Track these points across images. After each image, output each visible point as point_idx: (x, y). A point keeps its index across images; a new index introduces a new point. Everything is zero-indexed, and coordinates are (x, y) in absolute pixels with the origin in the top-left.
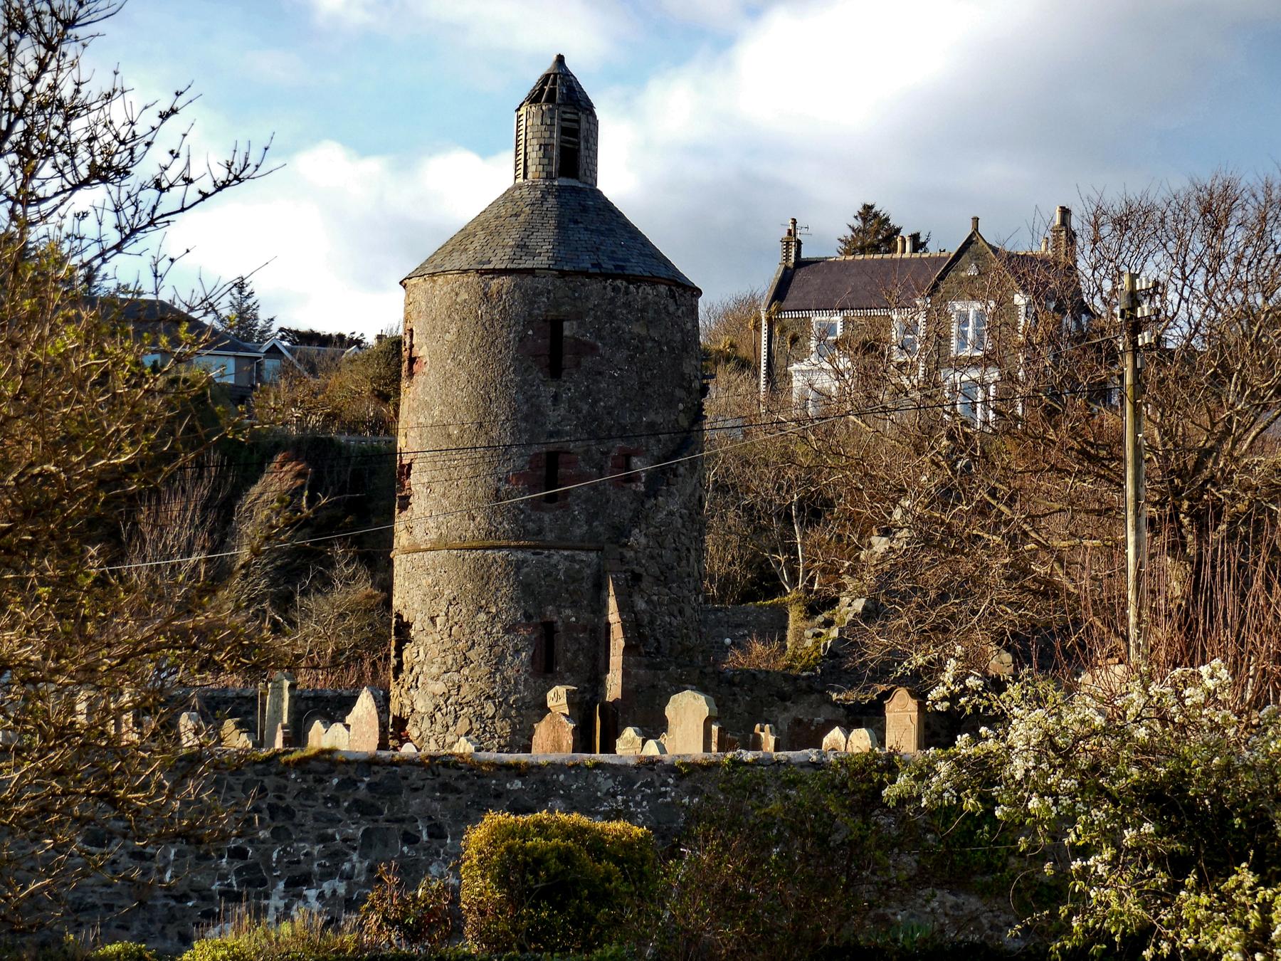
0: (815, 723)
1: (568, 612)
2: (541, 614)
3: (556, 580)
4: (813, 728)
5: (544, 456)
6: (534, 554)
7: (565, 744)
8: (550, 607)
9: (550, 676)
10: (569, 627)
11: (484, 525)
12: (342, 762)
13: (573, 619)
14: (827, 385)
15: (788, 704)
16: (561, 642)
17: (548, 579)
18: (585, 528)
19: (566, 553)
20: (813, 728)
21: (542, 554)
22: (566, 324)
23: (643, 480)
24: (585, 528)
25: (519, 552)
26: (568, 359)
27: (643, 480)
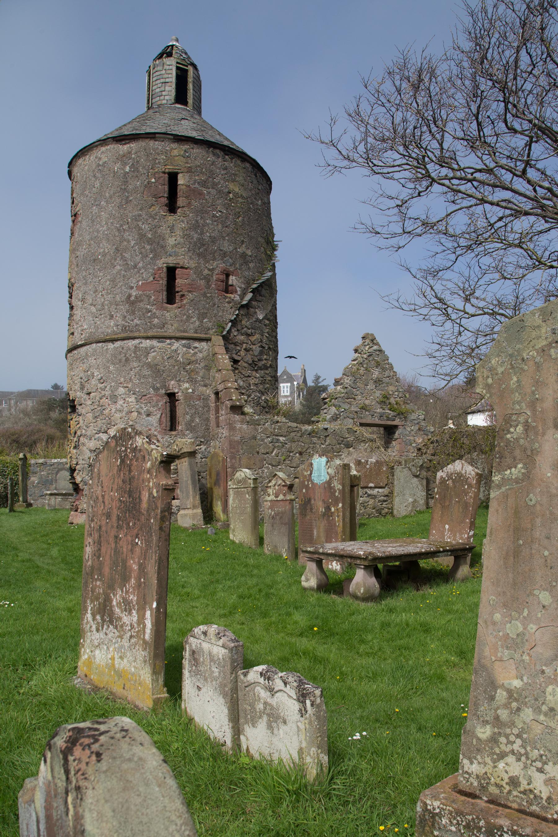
0: (369, 463)
1: (186, 385)
2: (164, 386)
3: (176, 361)
4: (368, 466)
5: (165, 270)
6: (158, 342)
7: (145, 496)
8: (173, 382)
9: (173, 433)
10: (188, 397)
11: (121, 322)
12: (486, 411)
13: (190, 391)
14: (61, 800)
15: (351, 449)
16: (180, 409)
17: (171, 361)
18: (197, 323)
19: (184, 342)
20: (368, 466)
21: (165, 342)
22: (180, 176)
23: (239, 293)
24: (197, 323)
25: (148, 341)
26: (181, 201)
27: (239, 293)
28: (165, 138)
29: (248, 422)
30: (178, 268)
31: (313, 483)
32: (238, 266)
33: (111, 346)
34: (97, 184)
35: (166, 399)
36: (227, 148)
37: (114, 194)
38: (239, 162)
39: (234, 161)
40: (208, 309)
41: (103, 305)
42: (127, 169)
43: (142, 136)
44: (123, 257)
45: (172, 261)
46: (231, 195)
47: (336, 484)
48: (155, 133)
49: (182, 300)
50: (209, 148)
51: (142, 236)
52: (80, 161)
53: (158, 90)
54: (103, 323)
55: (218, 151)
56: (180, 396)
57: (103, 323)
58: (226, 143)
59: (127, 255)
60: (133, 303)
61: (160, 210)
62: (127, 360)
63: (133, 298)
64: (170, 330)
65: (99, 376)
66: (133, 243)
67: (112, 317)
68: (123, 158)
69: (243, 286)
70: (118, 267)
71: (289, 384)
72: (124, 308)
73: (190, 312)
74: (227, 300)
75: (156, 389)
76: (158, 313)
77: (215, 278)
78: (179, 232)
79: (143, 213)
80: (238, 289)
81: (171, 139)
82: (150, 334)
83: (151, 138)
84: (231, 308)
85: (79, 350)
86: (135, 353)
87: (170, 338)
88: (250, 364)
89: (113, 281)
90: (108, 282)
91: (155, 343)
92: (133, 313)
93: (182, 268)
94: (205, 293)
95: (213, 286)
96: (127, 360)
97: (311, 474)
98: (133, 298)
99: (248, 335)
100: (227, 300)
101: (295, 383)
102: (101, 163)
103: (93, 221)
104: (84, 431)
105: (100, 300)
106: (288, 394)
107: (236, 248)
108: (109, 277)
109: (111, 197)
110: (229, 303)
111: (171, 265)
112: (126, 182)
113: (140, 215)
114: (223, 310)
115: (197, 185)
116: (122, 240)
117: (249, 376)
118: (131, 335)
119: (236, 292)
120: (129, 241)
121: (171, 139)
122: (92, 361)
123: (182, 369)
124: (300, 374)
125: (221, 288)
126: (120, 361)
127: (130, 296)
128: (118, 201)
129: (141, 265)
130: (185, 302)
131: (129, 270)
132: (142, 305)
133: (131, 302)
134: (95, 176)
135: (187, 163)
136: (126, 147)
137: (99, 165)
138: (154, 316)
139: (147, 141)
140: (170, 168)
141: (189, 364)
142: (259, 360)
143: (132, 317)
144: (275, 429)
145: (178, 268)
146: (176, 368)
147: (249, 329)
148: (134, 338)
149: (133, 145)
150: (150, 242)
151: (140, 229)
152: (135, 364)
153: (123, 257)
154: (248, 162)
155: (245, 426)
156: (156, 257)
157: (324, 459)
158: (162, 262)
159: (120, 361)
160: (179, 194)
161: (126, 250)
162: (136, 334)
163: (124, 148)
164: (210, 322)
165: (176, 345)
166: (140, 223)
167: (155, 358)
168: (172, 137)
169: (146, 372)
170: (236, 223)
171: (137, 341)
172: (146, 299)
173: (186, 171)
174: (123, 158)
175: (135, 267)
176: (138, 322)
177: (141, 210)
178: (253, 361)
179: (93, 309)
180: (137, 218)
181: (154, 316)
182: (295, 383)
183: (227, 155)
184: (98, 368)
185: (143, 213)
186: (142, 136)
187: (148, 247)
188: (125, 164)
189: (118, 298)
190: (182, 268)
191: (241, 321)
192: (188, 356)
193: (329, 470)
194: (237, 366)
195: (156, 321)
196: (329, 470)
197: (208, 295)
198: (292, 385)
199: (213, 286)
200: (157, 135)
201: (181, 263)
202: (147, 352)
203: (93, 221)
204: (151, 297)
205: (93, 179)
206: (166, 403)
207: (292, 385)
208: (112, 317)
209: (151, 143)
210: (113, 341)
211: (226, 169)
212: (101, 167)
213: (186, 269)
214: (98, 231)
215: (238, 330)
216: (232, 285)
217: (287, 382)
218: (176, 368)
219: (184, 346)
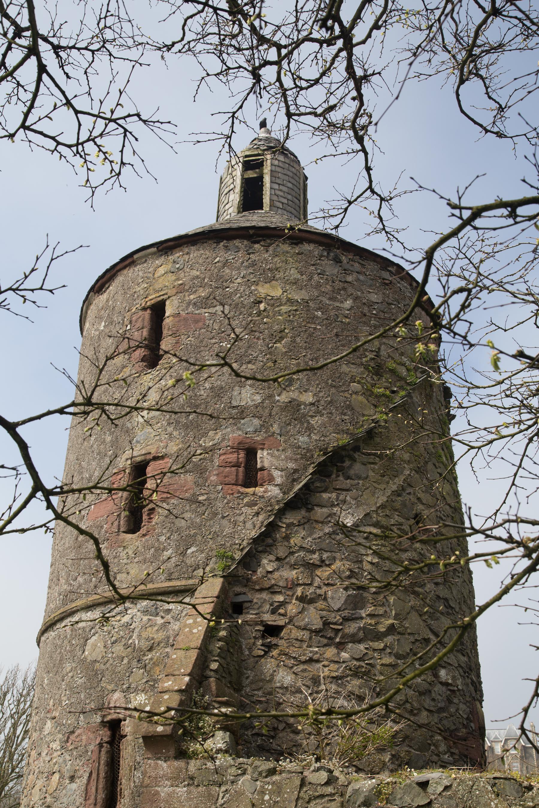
23: (279, 481)
28: (146, 256)
29: (192, 778)
30: (150, 460)
32: (275, 428)
35: (105, 734)
36: (251, 232)
38: (286, 247)
39: (271, 249)
40: (199, 527)
43: (118, 268)
46: (262, 306)
50: (218, 243)
55: (237, 242)
58: (312, 230)
69: (291, 465)
73: (162, 539)
74: (246, 500)
77: (217, 462)
80: (276, 474)
81: (153, 254)
83: (129, 265)
84: (257, 514)
88: (317, 632)
93: (156, 458)
94: (194, 494)
95: (213, 478)
99: (311, 567)
100: (246, 500)
107: (271, 396)
110: (251, 505)
111: (139, 459)
114: (235, 523)
115: (191, 309)
117: (311, 661)
119: (271, 479)
121: (153, 254)
123: (134, 663)
125: (232, 479)
135: (178, 279)
139: (125, 272)
140: (153, 298)
141: (151, 649)
142: (346, 619)
144: (263, 793)
145: (150, 460)
146: (125, 661)
147: (313, 552)
154: (310, 241)
155: (182, 790)
160: (165, 332)
164: (202, 552)
168: (154, 250)
170: (270, 351)
173: (174, 291)
178: (326, 624)
183: (258, 242)
186: (118, 268)
190: (156, 458)
191: (287, 538)
192: (151, 632)
194: (274, 641)
197: (201, 498)
199: (213, 478)
200: (135, 257)
201: (153, 451)
204: (102, 527)
206: (101, 745)
211: (253, 264)
213: (162, 458)
215: (278, 559)
216: (262, 469)
218: (125, 661)
219: (145, 612)
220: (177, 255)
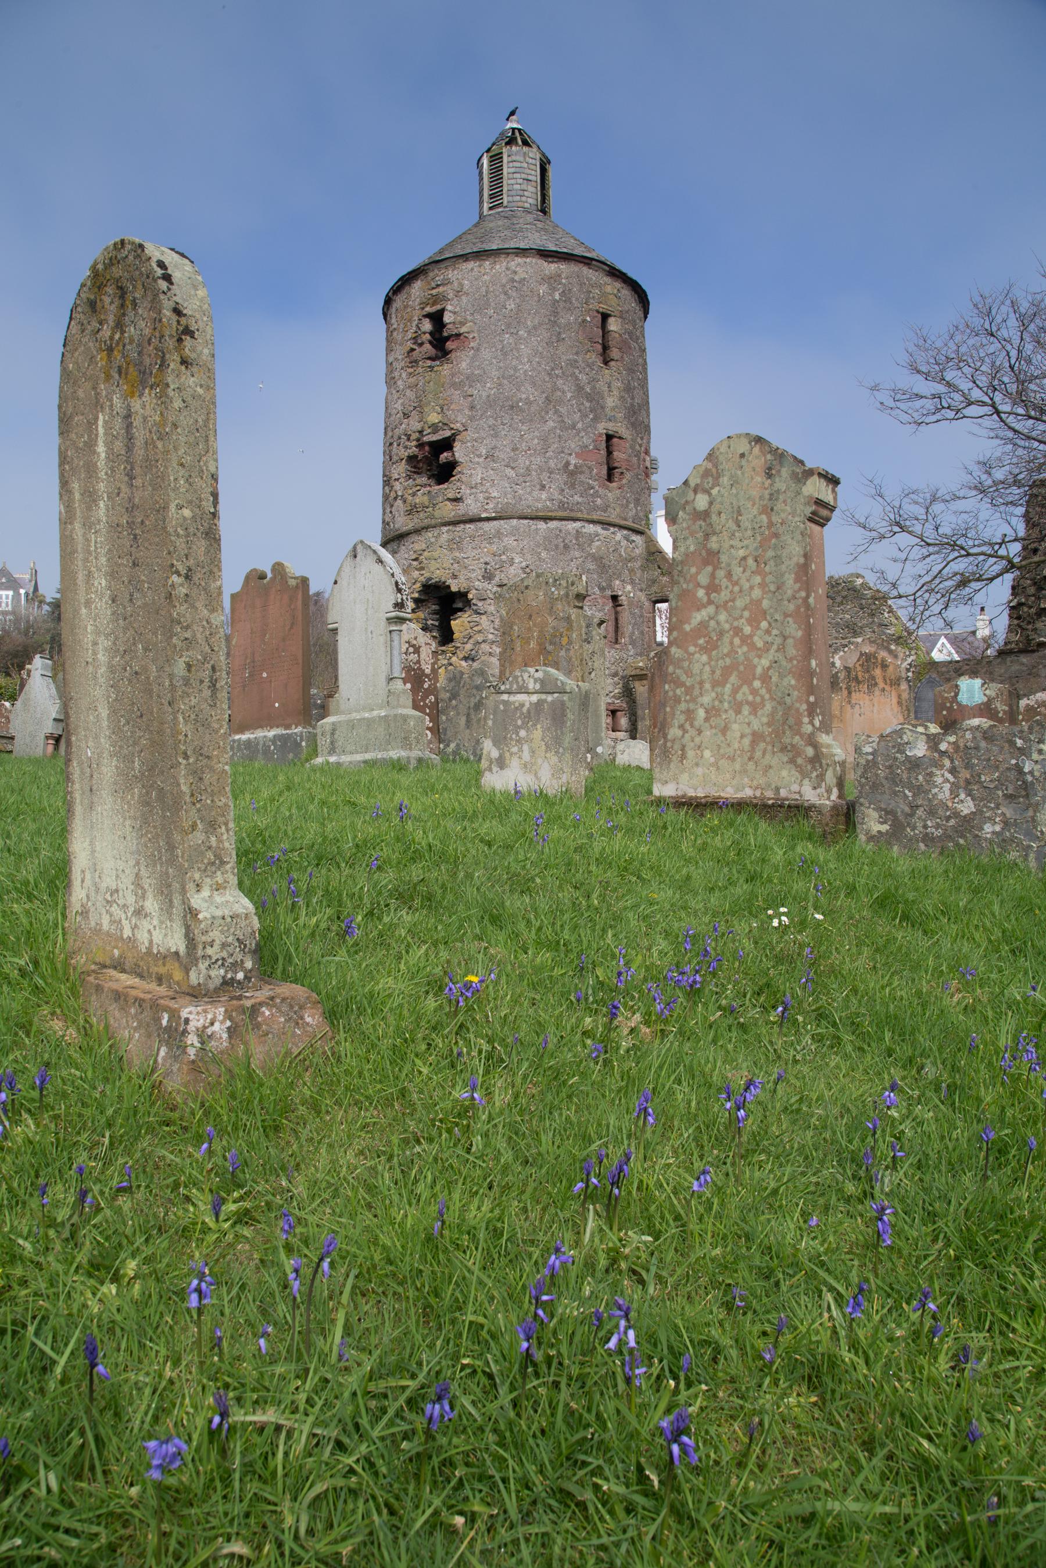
2: (610, 586)
11: (556, 496)
16: (625, 617)
26: (615, 353)
31: (959, 704)
33: (542, 525)
34: (511, 305)
37: (540, 324)
41: (528, 469)
42: (557, 297)
44: (556, 412)
45: (612, 427)
47: (998, 705)
48: (592, 259)
49: (621, 479)
51: (580, 389)
52: (471, 264)
53: (518, 187)
54: (530, 493)
56: (623, 599)
57: (530, 493)
59: (563, 410)
60: (572, 474)
61: (595, 358)
62: (566, 547)
63: (571, 467)
64: (613, 516)
65: (524, 564)
66: (569, 395)
67: (543, 487)
68: (552, 280)
70: (551, 424)
71: (11, 593)
72: (561, 478)
75: (602, 589)
76: (601, 491)
78: (616, 393)
79: (580, 359)
82: (595, 517)
85: (480, 524)
86: (577, 539)
87: (614, 525)
89: (544, 439)
90: (536, 441)
91: (598, 529)
92: (573, 486)
96: (566, 547)
97: (957, 695)
98: (571, 467)
101: (22, 591)
102: (517, 278)
103: (505, 354)
104: (491, 636)
105: (523, 462)
106: (10, 608)
108: (537, 433)
109: (535, 328)
112: (555, 313)
113: (576, 361)
116: (555, 388)
118: (573, 515)
120: (564, 392)
122: (510, 541)
124: (28, 577)
126: (557, 546)
127: (568, 464)
128: (546, 335)
129: (580, 425)
130: (624, 481)
131: (567, 429)
132: (582, 477)
133: (572, 474)
134: (506, 293)
136: (553, 267)
137: (513, 280)
138: (596, 495)
140: (604, 308)
143: (572, 492)
148: (575, 520)
149: (563, 266)
150: (590, 398)
151: (577, 379)
152: (577, 554)
153: (556, 412)
156: (596, 419)
157: (978, 682)
158: (602, 428)
159: (557, 546)
161: (560, 402)
162: (579, 515)
163: (551, 268)
165: (619, 535)
166: (577, 371)
167: (599, 548)
169: (591, 566)
171: (578, 524)
172: (587, 471)
174: (552, 280)
175: (574, 427)
176: (580, 500)
177: (577, 353)
179: (511, 473)
180: (573, 363)
181: (596, 495)
182: (22, 591)
184: (522, 553)
185: (580, 359)
187: (588, 405)
188: (554, 289)
189: (552, 464)
193: (988, 692)
195: (599, 501)
196: (988, 692)
198: (17, 595)
202: (591, 538)
203: (505, 354)
205: (502, 296)
207: (17, 595)
208: (543, 487)
209: (585, 270)
210: (546, 519)
212: (517, 284)
214: (516, 369)
217: (7, 589)
220: (618, 285)
